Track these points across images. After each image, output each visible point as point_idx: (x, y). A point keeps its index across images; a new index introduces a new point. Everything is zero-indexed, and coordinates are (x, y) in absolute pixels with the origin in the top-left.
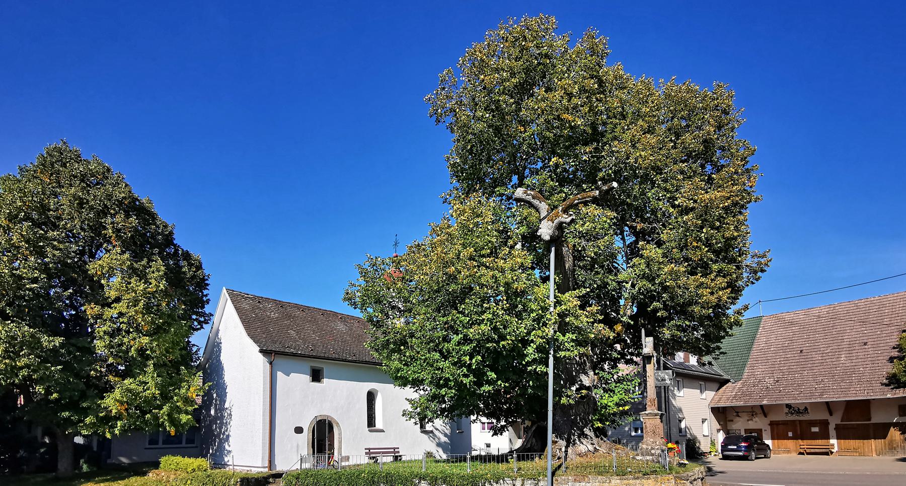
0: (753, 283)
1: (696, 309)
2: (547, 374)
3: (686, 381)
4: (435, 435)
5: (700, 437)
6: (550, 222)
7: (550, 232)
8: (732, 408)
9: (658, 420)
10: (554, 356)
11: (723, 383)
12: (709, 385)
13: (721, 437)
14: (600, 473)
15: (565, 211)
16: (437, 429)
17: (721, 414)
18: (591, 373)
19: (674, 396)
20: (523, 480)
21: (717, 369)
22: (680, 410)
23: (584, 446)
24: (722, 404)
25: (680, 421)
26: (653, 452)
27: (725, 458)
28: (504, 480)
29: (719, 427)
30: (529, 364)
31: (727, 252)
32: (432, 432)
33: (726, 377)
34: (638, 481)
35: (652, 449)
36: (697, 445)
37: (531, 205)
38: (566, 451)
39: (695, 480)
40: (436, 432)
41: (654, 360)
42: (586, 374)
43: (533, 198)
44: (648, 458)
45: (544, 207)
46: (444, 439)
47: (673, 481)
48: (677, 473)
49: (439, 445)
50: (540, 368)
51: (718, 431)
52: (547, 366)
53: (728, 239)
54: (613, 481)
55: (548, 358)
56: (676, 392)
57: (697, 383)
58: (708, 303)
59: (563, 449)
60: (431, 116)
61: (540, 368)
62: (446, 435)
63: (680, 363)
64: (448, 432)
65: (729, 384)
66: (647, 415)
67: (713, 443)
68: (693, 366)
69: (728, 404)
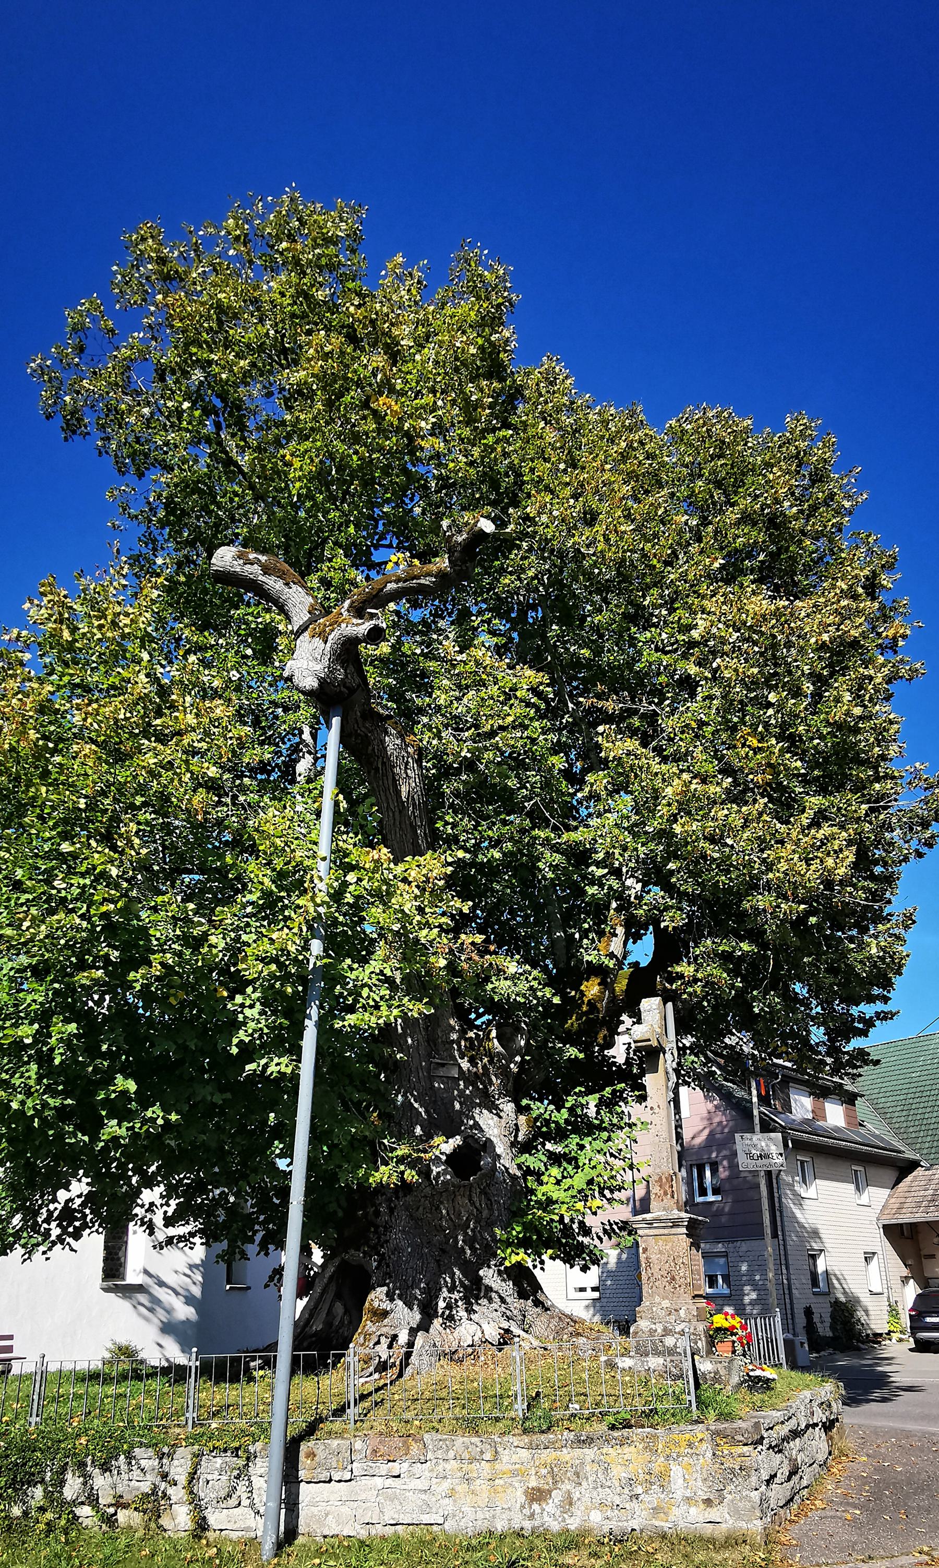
1: (763, 901)
2: (295, 1078)
3: (820, 1163)
4: (156, 1301)
5: (866, 1299)
6: (318, 641)
7: (320, 668)
8: (929, 1225)
9: (681, 1239)
10: (320, 1025)
11: (906, 1168)
12: (873, 1171)
13: (912, 1291)
14: (471, 1426)
15: (359, 612)
16: (161, 1284)
17: (905, 1237)
18: (508, 1108)
20: (198, 1456)
22: (815, 1234)
23: (479, 1325)
24: (906, 1218)
25: (814, 1257)
26: (670, 1341)
27: (923, 1347)
28: (130, 1457)
29: (905, 1272)
30: (248, 1052)
31: (841, 764)
32: (140, 1288)
33: (910, 1155)
34: (589, 1453)
35: (667, 1332)
36: (860, 1314)
38: (411, 1344)
40: (162, 1294)
42: (492, 1107)
43: (266, 570)
44: (655, 1362)
45: (299, 601)
46: (184, 1312)
47: (706, 1449)
48: (724, 1416)
49: (168, 1328)
50: (278, 1065)
51: (905, 1280)
52: (296, 1052)
54: (505, 1455)
55: (298, 1032)
56: (801, 1190)
57: (844, 1167)
59: (403, 1338)
61: (278, 1065)
62: (189, 1300)
63: (806, 1121)
64: (197, 1291)
65: (919, 1172)
66: (650, 1223)
67: (893, 1311)
68: (837, 1129)
69: (919, 1217)
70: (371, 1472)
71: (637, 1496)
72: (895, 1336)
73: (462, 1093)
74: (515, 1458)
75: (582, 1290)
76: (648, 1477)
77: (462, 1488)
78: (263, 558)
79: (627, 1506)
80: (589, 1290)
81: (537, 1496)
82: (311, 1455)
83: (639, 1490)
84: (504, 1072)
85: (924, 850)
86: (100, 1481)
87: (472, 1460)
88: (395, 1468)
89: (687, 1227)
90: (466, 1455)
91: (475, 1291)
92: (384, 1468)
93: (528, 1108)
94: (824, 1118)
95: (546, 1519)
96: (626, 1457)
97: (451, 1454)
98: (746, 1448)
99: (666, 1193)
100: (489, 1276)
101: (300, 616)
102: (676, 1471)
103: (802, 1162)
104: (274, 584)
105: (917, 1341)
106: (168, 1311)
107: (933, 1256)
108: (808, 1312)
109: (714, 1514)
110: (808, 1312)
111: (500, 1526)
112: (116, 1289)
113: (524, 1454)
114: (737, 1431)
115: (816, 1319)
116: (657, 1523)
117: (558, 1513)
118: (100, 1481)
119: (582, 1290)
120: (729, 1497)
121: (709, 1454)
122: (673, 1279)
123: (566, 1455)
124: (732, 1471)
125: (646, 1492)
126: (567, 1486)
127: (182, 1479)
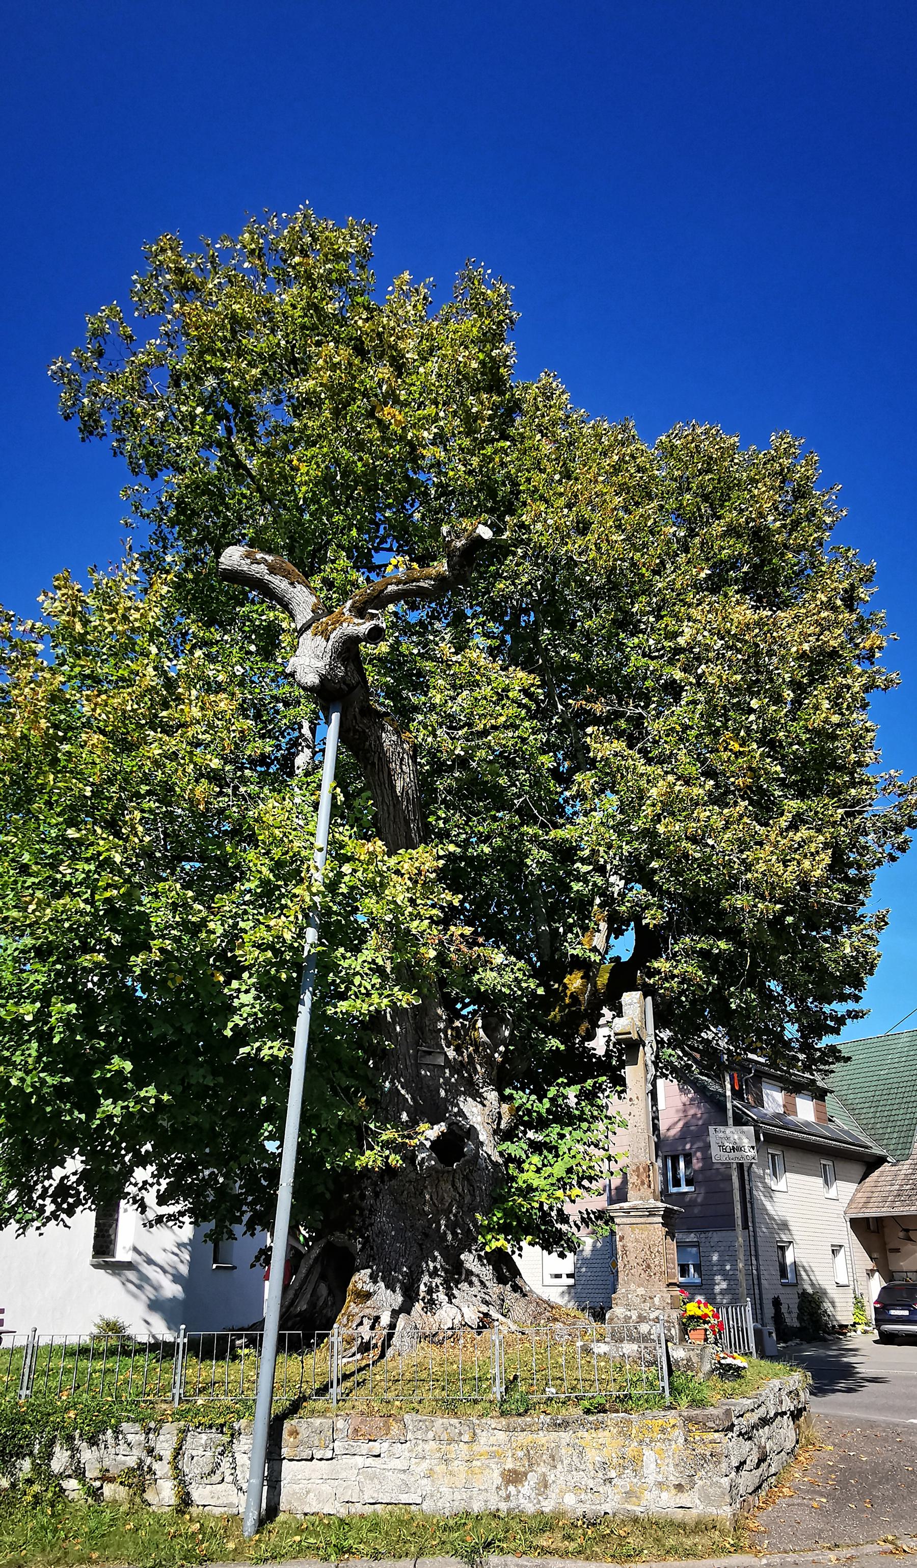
0: (893, 859)
1: (741, 900)
2: (288, 1061)
3: (791, 1157)
4: (144, 1278)
5: (832, 1291)
6: (320, 639)
7: (321, 665)
8: (896, 1219)
9: (658, 1230)
11: (873, 1163)
12: (841, 1166)
13: (876, 1284)
14: (450, 1407)
15: (360, 612)
16: (150, 1262)
17: (873, 1232)
18: (492, 1096)
19: (769, 1192)
21: (845, 1125)
22: (784, 1226)
24: (872, 1212)
25: (783, 1249)
26: (644, 1328)
27: (887, 1339)
28: (117, 1432)
29: (871, 1265)
30: (242, 1036)
31: (819, 769)
32: (129, 1266)
33: (877, 1151)
34: (565, 1436)
35: (642, 1319)
36: (827, 1305)
37: (267, 591)
38: (392, 1326)
39: (765, 1422)
41: (647, 1054)
42: (476, 1095)
43: (272, 570)
44: (629, 1348)
45: (303, 600)
46: (172, 1290)
47: (678, 1434)
49: (155, 1305)
50: (271, 1049)
51: (870, 1273)
52: (289, 1037)
53: (817, 733)
54: (483, 1437)
55: (292, 1017)
58: (773, 887)
59: (385, 1319)
60: (67, 418)
61: (271, 1049)
62: (177, 1278)
63: (777, 1116)
64: (184, 1270)
65: (886, 1167)
66: (627, 1212)
67: (859, 1303)
68: (807, 1124)
70: (352, 1451)
71: (610, 1480)
72: (860, 1328)
73: (447, 1081)
74: (492, 1440)
75: (558, 1276)
76: (621, 1461)
77: (440, 1469)
78: (270, 558)
79: (600, 1489)
80: (564, 1276)
81: (514, 1477)
82: (294, 1433)
83: (613, 1474)
84: (489, 1061)
85: (898, 854)
86: (87, 1455)
87: (451, 1441)
88: (376, 1447)
89: (663, 1217)
90: (445, 1436)
91: (456, 1274)
92: (365, 1448)
93: (511, 1098)
94: (795, 1113)
95: (522, 1501)
96: (600, 1441)
97: (431, 1435)
98: (716, 1435)
99: (643, 1183)
100: (469, 1260)
101: (303, 615)
102: (649, 1455)
103: (773, 1156)
104: (279, 583)
105: (881, 1333)
106: (156, 1288)
107: (897, 1250)
108: (777, 1303)
109: (684, 1499)
110: (777, 1303)
111: (477, 1507)
112: (106, 1266)
113: (502, 1436)
114: (710, 1418)
115: (784, 1309)
116: (629, 1507)
117: (533, 1496)
118: (87, 1455)
119: (558, 1276)
120: (700, 1483)
121: (681, 1440)
122: (649, 1267)
123: (543, 1438)
124: (703, 1457)
125: (619, 1476)
126: (542, 1469)
127: (168, 1454)
